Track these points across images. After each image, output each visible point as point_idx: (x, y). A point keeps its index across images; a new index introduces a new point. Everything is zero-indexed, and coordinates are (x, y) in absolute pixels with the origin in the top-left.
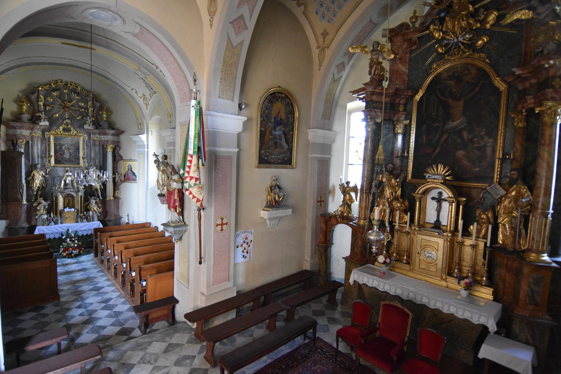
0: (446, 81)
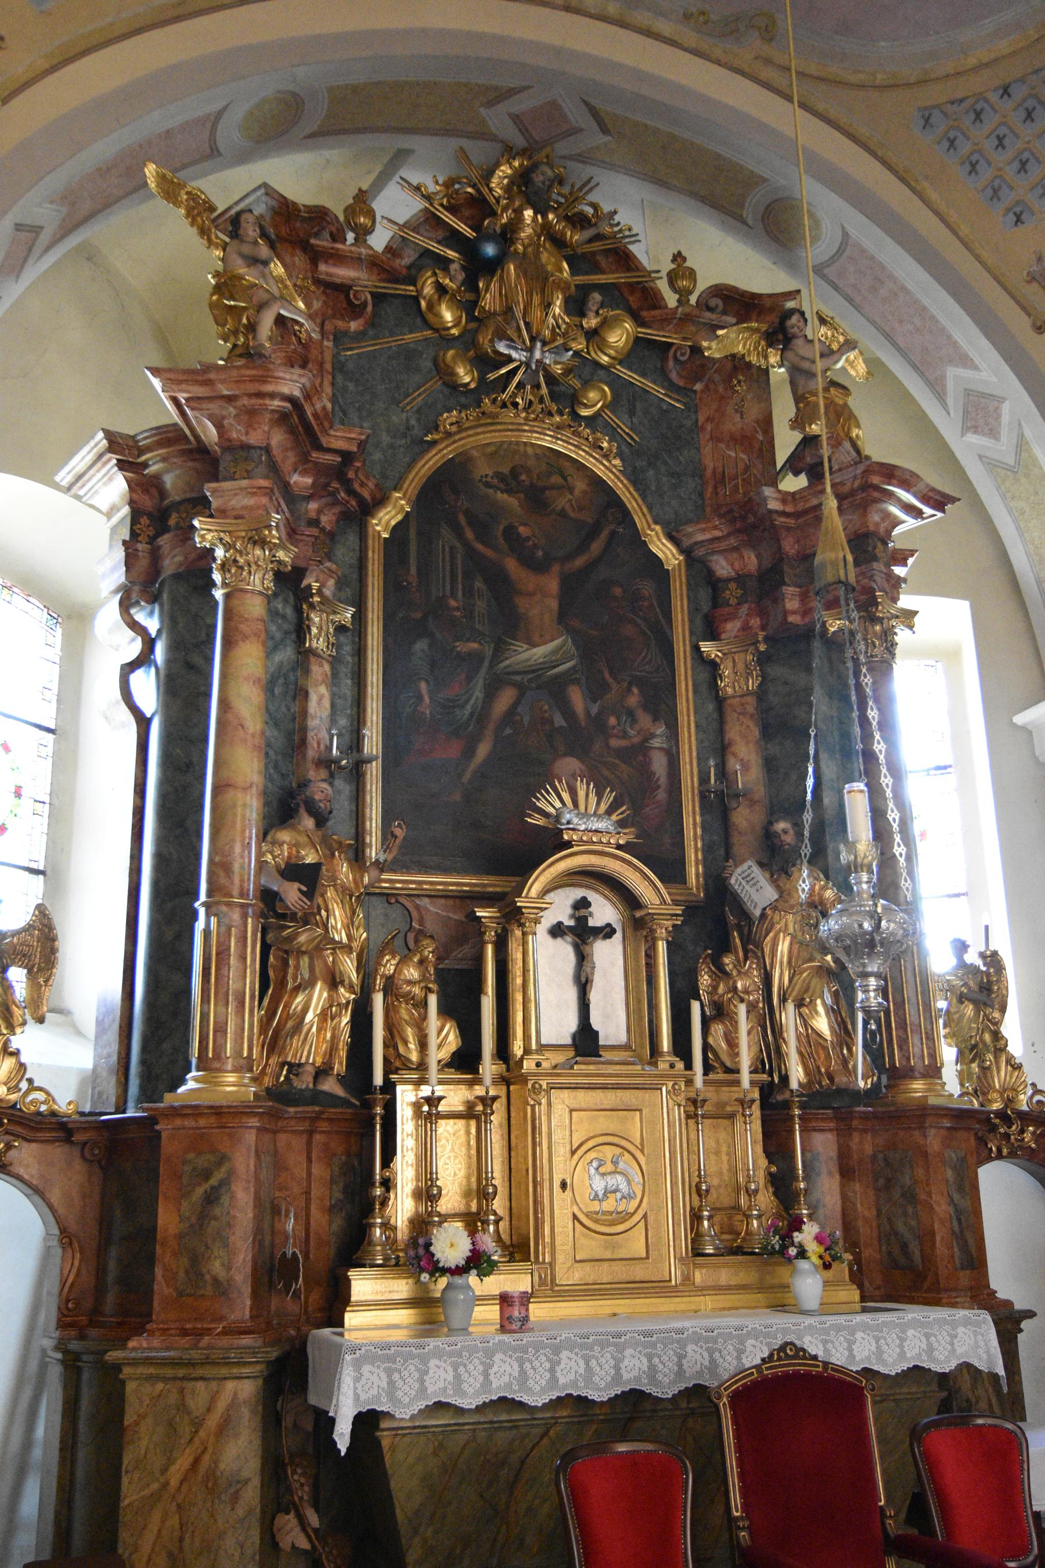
0: (492, 491)
